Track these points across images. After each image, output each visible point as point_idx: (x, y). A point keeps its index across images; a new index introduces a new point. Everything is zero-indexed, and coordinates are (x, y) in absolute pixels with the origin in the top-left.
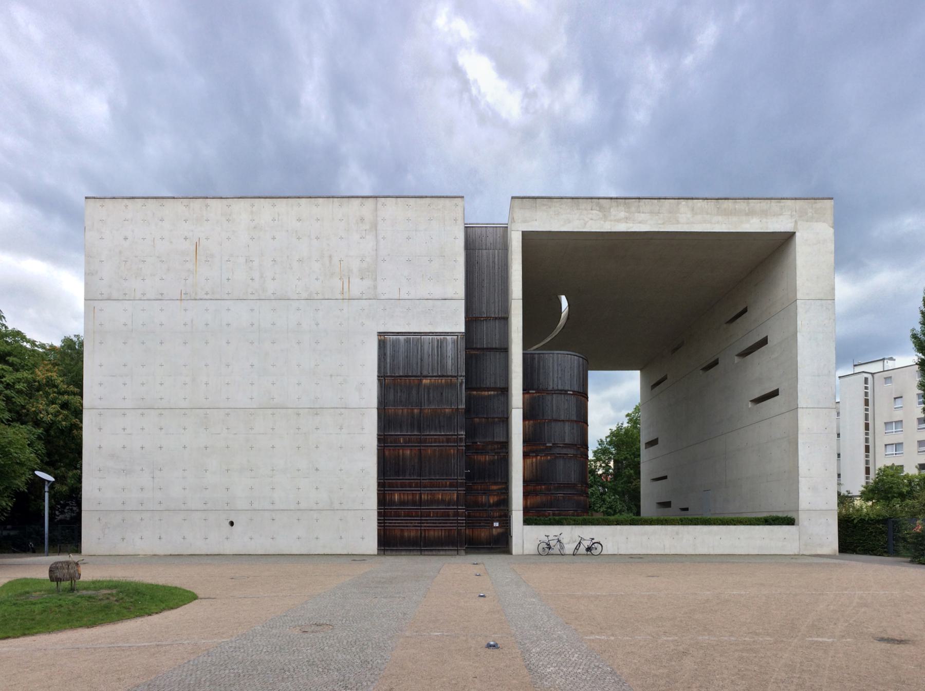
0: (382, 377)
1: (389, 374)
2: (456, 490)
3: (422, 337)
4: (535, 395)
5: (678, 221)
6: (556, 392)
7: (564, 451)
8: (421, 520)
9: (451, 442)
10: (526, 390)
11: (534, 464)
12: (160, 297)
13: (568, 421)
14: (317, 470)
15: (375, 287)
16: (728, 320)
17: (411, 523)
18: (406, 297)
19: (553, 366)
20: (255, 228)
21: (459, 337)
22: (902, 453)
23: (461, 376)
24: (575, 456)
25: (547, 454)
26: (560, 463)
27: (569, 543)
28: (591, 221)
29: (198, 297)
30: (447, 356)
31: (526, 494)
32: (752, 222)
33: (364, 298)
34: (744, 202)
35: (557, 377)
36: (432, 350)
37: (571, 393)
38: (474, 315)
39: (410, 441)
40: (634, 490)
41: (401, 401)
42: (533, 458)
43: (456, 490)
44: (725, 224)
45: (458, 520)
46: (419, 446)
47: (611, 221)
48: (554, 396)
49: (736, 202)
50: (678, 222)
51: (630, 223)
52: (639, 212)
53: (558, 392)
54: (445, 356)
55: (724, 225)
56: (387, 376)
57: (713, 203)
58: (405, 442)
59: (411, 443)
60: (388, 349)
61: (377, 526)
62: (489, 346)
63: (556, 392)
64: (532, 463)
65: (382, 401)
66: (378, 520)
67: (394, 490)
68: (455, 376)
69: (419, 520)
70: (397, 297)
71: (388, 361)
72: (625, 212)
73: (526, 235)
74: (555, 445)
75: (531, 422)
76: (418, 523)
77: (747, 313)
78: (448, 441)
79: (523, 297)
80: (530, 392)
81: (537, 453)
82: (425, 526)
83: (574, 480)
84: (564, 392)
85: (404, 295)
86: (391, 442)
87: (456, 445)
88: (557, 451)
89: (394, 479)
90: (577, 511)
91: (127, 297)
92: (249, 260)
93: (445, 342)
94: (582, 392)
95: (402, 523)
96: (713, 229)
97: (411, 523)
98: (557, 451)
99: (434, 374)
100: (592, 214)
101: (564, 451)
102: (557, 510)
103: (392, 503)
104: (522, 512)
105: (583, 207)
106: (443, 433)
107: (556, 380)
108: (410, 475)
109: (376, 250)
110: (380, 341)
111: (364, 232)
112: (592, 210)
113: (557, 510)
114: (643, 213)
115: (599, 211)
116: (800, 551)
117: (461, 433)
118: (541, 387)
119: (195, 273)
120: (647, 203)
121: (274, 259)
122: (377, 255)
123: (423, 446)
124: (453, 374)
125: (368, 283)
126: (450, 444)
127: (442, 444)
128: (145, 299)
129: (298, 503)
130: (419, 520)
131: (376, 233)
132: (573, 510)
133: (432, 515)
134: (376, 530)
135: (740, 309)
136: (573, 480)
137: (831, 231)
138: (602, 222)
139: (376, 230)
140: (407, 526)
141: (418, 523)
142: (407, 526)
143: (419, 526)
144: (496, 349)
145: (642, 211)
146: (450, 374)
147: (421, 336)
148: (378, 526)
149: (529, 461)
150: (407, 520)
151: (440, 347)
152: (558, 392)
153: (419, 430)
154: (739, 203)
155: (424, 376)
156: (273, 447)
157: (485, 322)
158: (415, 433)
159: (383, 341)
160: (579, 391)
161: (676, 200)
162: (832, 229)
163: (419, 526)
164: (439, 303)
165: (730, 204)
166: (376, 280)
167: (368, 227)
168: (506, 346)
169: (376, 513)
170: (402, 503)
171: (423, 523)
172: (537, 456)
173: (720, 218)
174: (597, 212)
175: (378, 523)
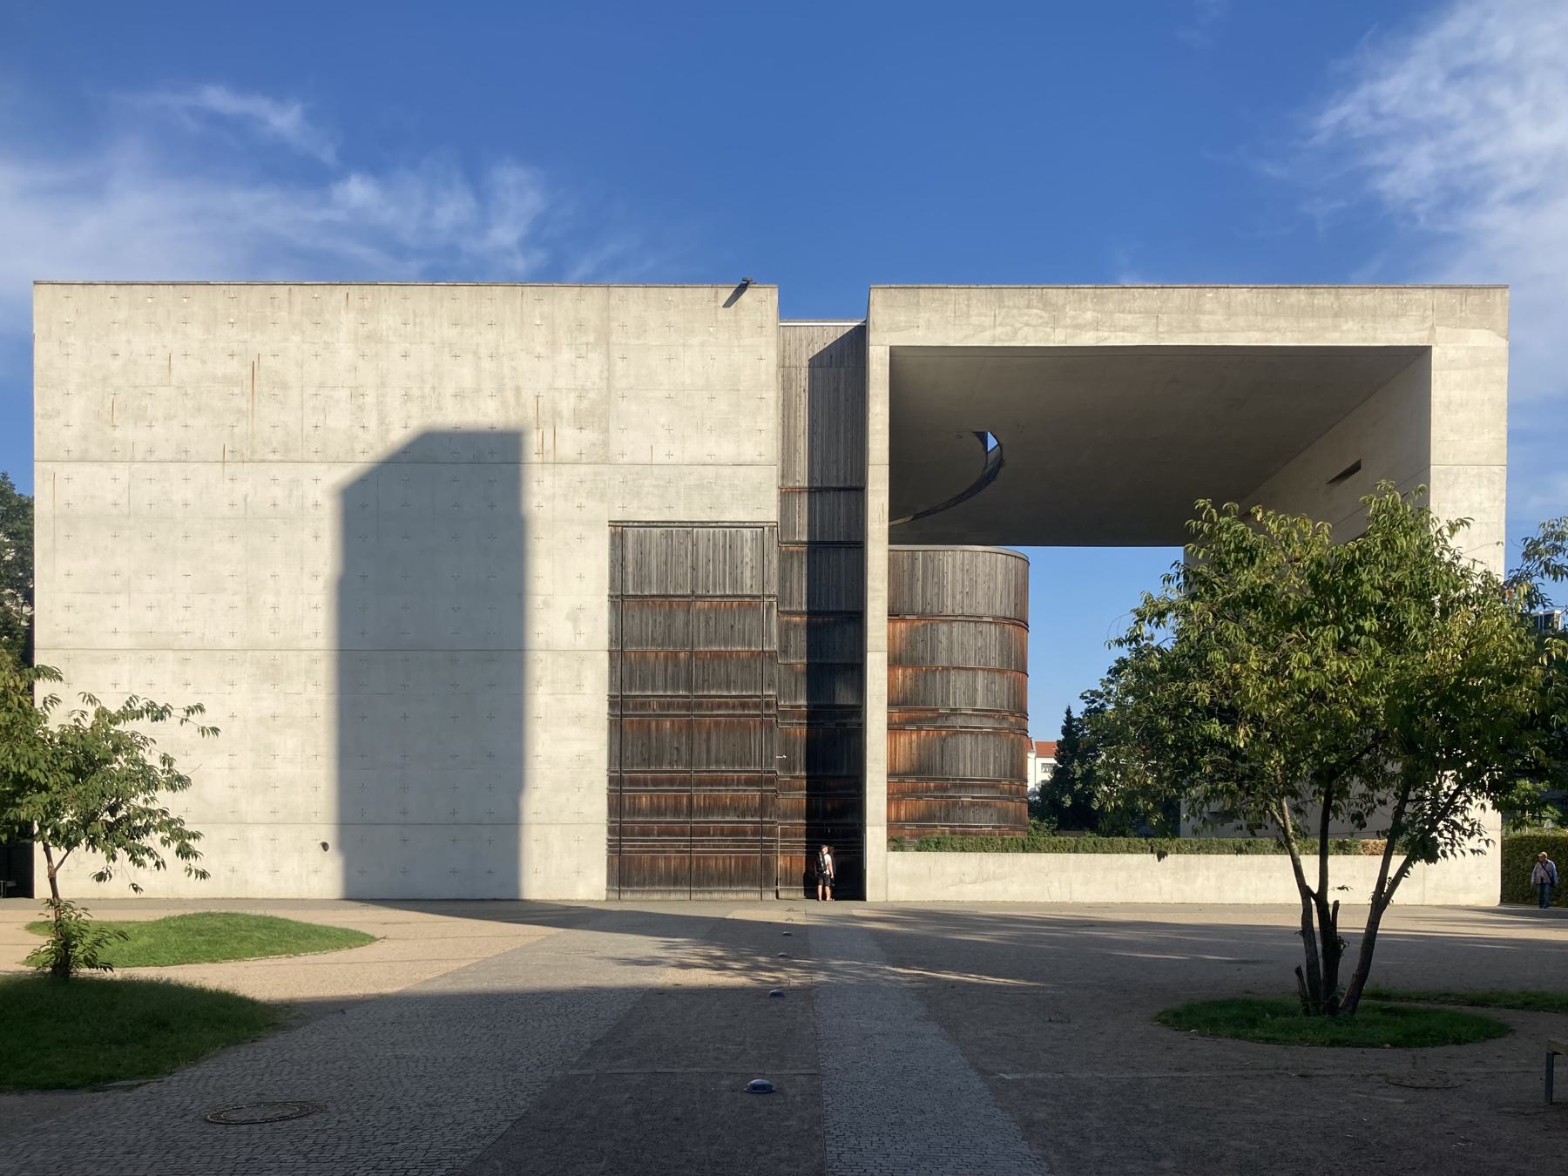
0: (617, 597)
1: (631, 593)
2: (759, 790)
3: (695, 530)
4: (916, 623)
5: (1197, 326)
6: (959, 618)
7: (975, 722)
8: (691, 841)
9: (749, 709)
10: (894, 614)
11: (914, 745)
12: (183, 457)
13: (983, 670)
14: (490, 755)
15: (606, 444)
16: (1330, 479)
17: (672, 846)
18: (666, 460)
19: (954, 573)
20: (368, 337)
21: (766, 529)
22: (83, 701)
23: (769, 596)
24: (996, 732)
25: (941, 727)
26: (967, 743)
27: (975, 882)
28: (1026, 328)
29: (256, 458)
30: (742, 562)
31: (893, 798)
32: (1345, 328)
33: (584, 461)
34: (1330, 294)
35: (962, 592)
36: (714, 552)
37: (991, 620)
38: (797, 484)
39: (670, 706)
40: (144, 407)
41: (654, 639)
42: (911, 734)
43: (759, 790)
44: (1292, 331)
45: (762, 841)
46: (688, 716)
47: (1066, 327)
48: (955, 625)
49: (1315, 294)
50: (1197, 329)
51: (1105, 331)
52: (1123, 312)
53: (963, 618)
54: (739, 562)
55: (1289, 333)
56: (628, 596)
57: (1268, 295)
58: (661, 706)
59: (674, 709)
60: (630, 550)
61: (606, 852)
62: (826, 539)
63: (959, 618)
64: (911, 743)
65: (617, 639)
66: (609, 840)
67: (640, 791)
68: (759, 597)
69: (687, 841)
70: (647, 460)
71: (630, 570)
72: (1094, 311)
73: (895, 352)
74: (955, 712)
75: (910, 671)
76: (685, 847)
77: (1360, 472)
78: (743, 706)
79: (890, 462)
80: (908, 617)
81: (917, 723)
82: (699, 852)
83: (995, 773)
84: (976, 619)
85: (660, 457)
86: (635, 708)
87: (758, 713)
88: (960, 721)
89: (641, 772)
90: (999, 827)
91: (119, 456)
92: (356, 393)
93: (739, 538)
94: (1012, 617)
95: (654, 846)
96: (1266, 341)
97: (672, 846)
98: (960, 721)
99: (718, 593)
100: (1030, 316)
101: (975, 722)
102: (960, 826)
103: (637, 811)
104: (886, 828)
105: (1011, 304)
106: (734, 693)
107: (959, 597)
108: (671, 764)
109: (608, 378)
110: (613, 536)
111: (585, 346)
112: (1028, 307)
113: (960, 826)
114: (1130, 312)
115: (1043, 309)
116: (1424, 900)
117: (768, 693)
118: (928, 610)
119: (250, 416)
120: (1137, 295)
121: (406, 392)
122: (609, 387)
123: (695, 716)
124: (755, 593)
125: (590, 435)
126: (746, 712)
127: (731, 712)
128: (152, 460)
129: (454, 813)
130: (687, 841)
131: (608, 351)
132: (993, 827)
133: (711, 832)
134: (606, 858)
135: (1348, 465)
136: (991, 773)
137: (1504, 343)
138: (1048, 330)
139: (608, 344)
140: (665, 852)
141: (685, 847)
142: (665, 852)
143: (687, 852)
144: (839, 543)
145: (1127, 308)
146: (749, 593)
147: (693, 527)
148: (609, 852)
149: (903, 739)
150: (665, 840)
151: (730, 547)
152: (963, 618)
153: (689, 687)
154: (1320, 294)
155: (697, 597)
156: (405, 717)
157: (818, 494)
158: (681, 693)
159: (619, 531)
160: (1008, 615)
161: (1196, 290)
162: (1504, 341)
163: (687, 852)
164: (728, 471)
165: (1303, 297)
166: (607, 430)
167: (591, 339)
168: (859, 539)
169: (605, 829)
170: (657, 811)
171: (695, 846)
172: (919, 729)
173: (1282, 323)
174: (1039, 311)
175: (610, 846)
